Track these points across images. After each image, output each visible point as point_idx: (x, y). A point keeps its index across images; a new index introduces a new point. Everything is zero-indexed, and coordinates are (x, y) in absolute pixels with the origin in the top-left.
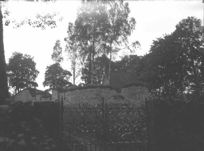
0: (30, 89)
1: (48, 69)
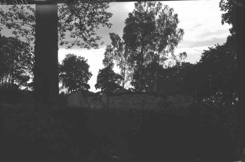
0: (82, 90)
1: (100, 72)
